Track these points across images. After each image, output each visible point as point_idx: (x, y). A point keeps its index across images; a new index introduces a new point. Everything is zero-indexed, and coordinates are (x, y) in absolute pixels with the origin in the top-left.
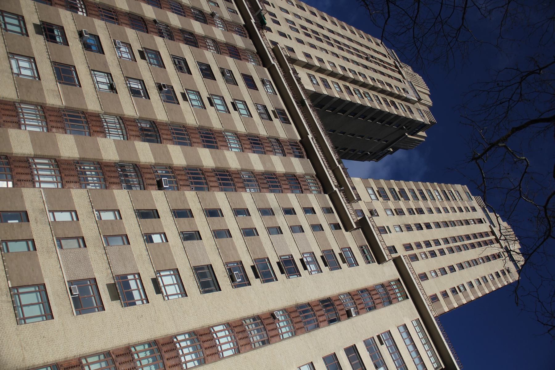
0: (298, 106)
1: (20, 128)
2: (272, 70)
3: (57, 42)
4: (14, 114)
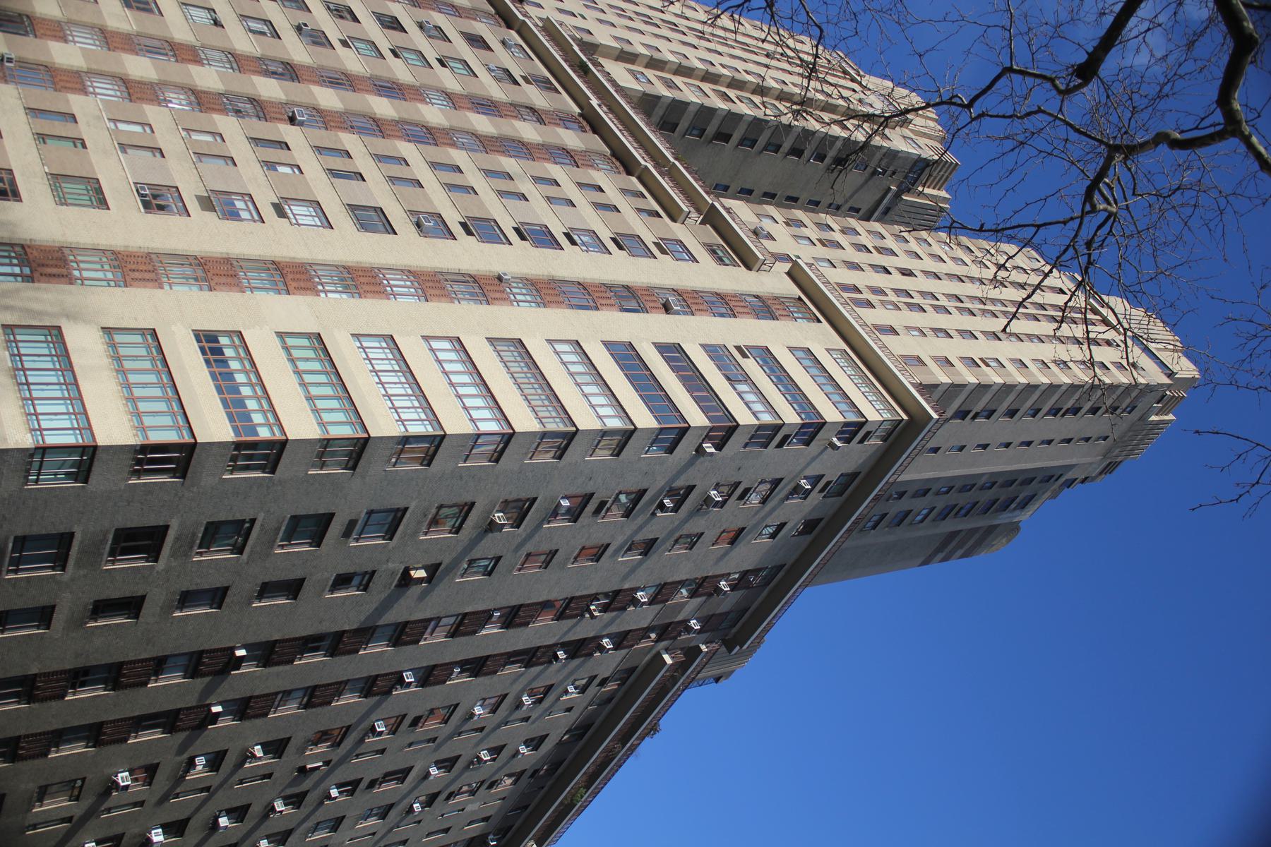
0: (579, 76)
1: (162, 288)
2: (644, 177)
3: (242, 220)
4: (150, 268)
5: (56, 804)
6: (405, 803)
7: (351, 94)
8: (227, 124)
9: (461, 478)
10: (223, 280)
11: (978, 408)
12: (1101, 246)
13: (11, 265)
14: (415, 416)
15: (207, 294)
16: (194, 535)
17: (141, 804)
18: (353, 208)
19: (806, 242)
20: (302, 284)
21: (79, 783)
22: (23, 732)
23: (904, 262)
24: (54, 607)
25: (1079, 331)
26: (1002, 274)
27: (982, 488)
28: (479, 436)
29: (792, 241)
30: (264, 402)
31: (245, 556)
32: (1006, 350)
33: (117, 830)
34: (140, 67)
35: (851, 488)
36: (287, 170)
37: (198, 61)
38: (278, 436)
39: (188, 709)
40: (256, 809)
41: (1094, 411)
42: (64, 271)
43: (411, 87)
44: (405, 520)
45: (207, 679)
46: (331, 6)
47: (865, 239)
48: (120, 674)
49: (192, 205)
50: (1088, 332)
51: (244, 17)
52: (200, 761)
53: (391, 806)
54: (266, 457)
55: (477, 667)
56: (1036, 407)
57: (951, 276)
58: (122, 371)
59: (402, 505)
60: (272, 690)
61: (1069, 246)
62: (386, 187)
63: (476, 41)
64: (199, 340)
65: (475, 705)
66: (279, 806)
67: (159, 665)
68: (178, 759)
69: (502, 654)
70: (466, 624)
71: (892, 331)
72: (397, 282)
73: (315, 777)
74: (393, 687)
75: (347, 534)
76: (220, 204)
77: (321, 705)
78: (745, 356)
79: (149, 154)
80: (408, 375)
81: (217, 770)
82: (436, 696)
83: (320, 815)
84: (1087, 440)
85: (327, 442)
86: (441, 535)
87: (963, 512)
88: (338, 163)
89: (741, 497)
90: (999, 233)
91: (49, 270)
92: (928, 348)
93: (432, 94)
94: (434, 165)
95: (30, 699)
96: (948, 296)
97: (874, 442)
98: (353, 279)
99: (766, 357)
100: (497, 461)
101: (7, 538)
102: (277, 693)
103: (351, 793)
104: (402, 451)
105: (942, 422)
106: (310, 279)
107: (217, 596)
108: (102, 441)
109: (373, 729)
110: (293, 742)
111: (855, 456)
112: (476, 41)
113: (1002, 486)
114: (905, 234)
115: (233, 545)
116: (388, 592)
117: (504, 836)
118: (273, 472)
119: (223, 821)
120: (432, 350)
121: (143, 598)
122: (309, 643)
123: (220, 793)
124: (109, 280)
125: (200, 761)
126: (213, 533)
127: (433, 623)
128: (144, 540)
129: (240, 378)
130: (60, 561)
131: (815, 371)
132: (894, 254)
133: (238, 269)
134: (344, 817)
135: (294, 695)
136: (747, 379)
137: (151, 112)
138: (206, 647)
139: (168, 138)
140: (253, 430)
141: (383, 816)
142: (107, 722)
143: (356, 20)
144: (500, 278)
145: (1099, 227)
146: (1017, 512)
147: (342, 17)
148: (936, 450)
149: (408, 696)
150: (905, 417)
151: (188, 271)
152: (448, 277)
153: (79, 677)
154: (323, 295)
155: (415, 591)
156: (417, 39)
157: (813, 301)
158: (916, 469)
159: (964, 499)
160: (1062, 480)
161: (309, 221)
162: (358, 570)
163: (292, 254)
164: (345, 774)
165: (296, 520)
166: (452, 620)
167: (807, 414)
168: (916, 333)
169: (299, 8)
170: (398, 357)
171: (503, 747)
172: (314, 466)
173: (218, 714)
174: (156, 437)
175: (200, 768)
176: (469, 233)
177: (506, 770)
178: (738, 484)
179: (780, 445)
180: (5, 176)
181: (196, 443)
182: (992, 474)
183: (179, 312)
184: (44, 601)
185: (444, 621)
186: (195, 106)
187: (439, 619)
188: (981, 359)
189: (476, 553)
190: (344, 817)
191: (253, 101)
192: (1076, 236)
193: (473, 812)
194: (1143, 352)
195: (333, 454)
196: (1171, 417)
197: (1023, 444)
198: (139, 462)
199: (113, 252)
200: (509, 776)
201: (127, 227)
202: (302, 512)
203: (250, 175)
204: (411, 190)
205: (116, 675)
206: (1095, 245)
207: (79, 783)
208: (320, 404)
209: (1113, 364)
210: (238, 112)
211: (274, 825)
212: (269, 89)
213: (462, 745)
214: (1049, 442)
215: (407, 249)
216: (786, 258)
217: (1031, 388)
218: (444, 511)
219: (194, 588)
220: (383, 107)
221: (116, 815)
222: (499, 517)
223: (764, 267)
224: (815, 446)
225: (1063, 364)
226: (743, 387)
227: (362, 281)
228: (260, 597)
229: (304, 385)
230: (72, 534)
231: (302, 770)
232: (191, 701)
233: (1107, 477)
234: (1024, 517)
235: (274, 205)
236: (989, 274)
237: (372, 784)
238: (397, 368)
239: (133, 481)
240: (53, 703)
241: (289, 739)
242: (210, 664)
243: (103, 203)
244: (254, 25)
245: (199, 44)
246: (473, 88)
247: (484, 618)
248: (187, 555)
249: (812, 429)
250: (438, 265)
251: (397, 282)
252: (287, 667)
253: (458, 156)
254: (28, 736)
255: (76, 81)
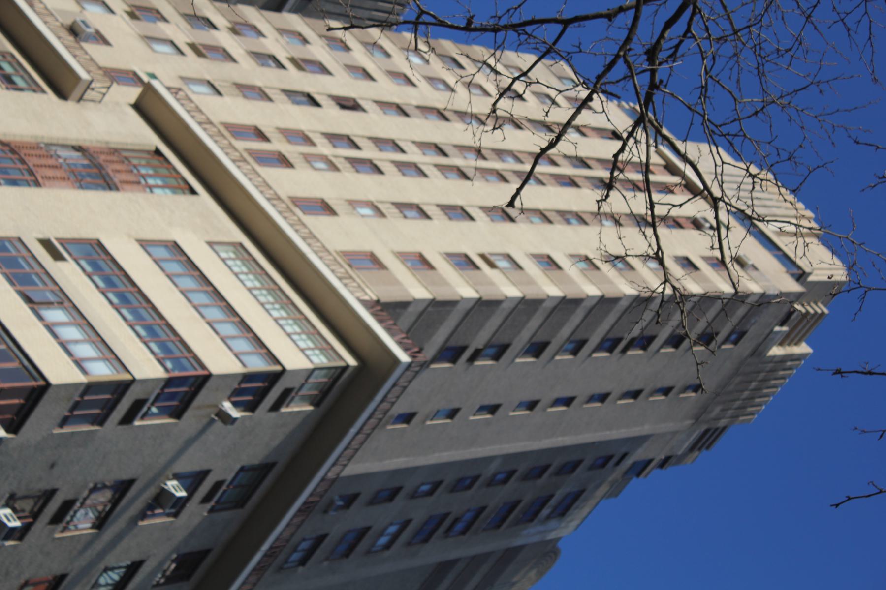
11: (479, 342)
12: (673, 56)
19: (167, 49)
23: (343, 84)
25: (638, 203)
26: (505, 104)
27: (492, 482)
29: (140, 47)
32: (523, 239)
35: (258, 492)
41: (676, 341)
47: (273, 44)
50: (652, 205)
56: (579, 336)
57: (426, 110)
61: (617, 56)
71: (326, 208)
78: (57, 256)
84: (666, 391)
87: (459, 526)
89: (58, 518)
90: (502, 31)
92: (388, 238)
96: (424, 146)
97: (299, 407)
99: (96, 257)
105: (417, 368)
111: (260, 435)
113: (526, 477)
114: (339, 34)
131: (188, 283)
132: (229, 57)
136: (64, 300)
145: (669, 24)
146: (553, 523)
148: (407, 418)
150: (352, 362)
157: (182, 156)
158: (374, 454)
159: (459, 504)
160: (628, 462)
167: (176, 361)
168: (367, 211)
178: (49, 494)
179: (128, 419)
182: (507, 458)
188: (483, 256)
192: (628, 40)
194: (750, 237)
196: (803, 348)
197: (557, 402)
206: (662, 56)
209: (694, 260)
214: (603, 398)
216: (133, 78)
217: (568, 304)
223: (89, 94)
224: (192, 418)
225: (618, 260)
226: (55, 315)
233: (703, 456)
234: (564, 531)
236: (482, 106)
249: (186, 388)
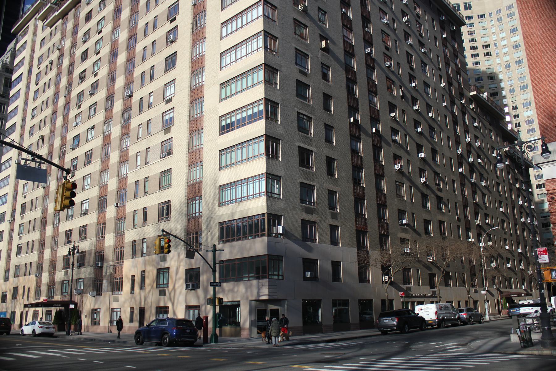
4: (194, 152)
5: (404, 192)
6: (421, 55)
7: (117, 72)
8: (134, 123)
9: (283, 24)
10: (198, 124)
13: (195, 204)
14: (256, 43)
15: (205, 130)
16: (303, 136)
17: (408, 161)
18: (166, 71)
20: (200, 91)
21: (398, 183)
22: (376, 202)
24: (329, 190)
28: (264, 15)
30: (249, 107)
31: (312, 116)
33: (417, 170)
34: (114, 157)
36: (152, 98)
37: (109, 135)
38: (263, 101)
39: (373, 142)
40: (416, 117)
42: (197, 184)
43: (112, 46)
44: (300, 49)
45: (362, 133)
46: (80, 81)
48: (357, 167)
49: (168, 136)
51: (89, 117)
52: (394, 138)
53: (422, 62)
54: (272, 107)
55: (366, 20)
58: (236, 163)
59: (294, 50)
60: (368, 108)
62: (156, 56)
63: (89, 16)
64: (223, 133)
65: (382, 22)
66: (416, 108)
67: (354, 152)
68: (392, 146)
69: (361, 8)
70: (347, 24)
72: (197, 51)
73: (406, 92)
74: (372, 58)
75: (305, 74)
76: (167, 125)
77: (376, 88)
79: (149, 153)
80: (237, 46)
81: (399, 131)
82: (377, 39)
83: (422, 92)
85: (266, 82)
86: (307, 34)
88: (147, 77)
91: (197, 190)
93: (106, 130)
94: (145, 35)
95: (363, 199)
98: (197, 70)
100: (276, 7)
101: (301, 206)
102: (370, 106)
103: (414, 78)
104: (270, 49)
106: (197, 88)
107: (328, 128)
108: (264, 171)
109: (389, 67)
110: (391, 101)
112: (89, 16)
115: (308, 121)
116: (331, 58)
117: (441, 13)
118: (278, 104)
119: (419, 130)
120: (227, 36)
121: (327, 157)
122: (350, 92)
123: (408, 130)
124: (200, 168)
125: (394, 138)
126: (303, 129)
127: (345, 39)
128: (304, 157)
129: (239, 117)
130: (311, 187)
133: (194, 118)
134: (424, 81)
135: (371, 99)
137: (132, 152)
138: (349, 133)
139: (141, 146)
140: (260, 112)
141: (426, 65)
142: (375, 172)
143: (85, 71)
144: (194, 5)
147: (85, 77)
149: (374, 51)
151: (195, 138)
152: (195, 29)
153: (356, 182)
154: (204, 83)
155: (331, 46)
156: (90, 44)
161: (172, 89)
162: (321, 70)
163: (187, 96)
164: (406, 80)
165: (298, 95)
166: (345, 31)
169: (83, 94)
170: (230, 51)
171: (402, 11)
172: (276, 87)
173: (376, 130)
174: (263, 150)
175: (397, 138)
176: (175, 19)
177: (413, 10)
180: (161, 206)
181: (268, 255)
183: (212, 141)
184: (326, 194)
185: (345, 34)
186: (128, 135)
187: (344, 36)
189: (316, 19)
190: (424, 81)
191: (124, 112)
193: (429, 26)
195: (271, 80)
198: (273, 157)
199: (189, 166)
200: (415, 9)
201: (178, 161)
202: (295, 93)
203: (155, 114)
204: (157, 46)
205: (357, 168)
207: (398, 183)
208: (250, 84)
210: (129, 118)
211: (423, 110)
212: (118, 106)
213: (399, 29)
215: (183, 46)
218: (297, 32)
219: (324, 137)
220: (122, 58)
221: (411, 170)
222: (301, 7)
227: (197, 66)
228: (329, 111)
229: (242, 91)
230: (301, 182)
231: (402, 97)
232: (370, 140)
235: (166, 103)
237: (412, 69)
238: (234, 51)
239: (280, 159)
240: (366, 191)
241: (389, 102)
242: (356, 133)
243: (170, 170)
244: (92, 113)
245: (102, 135)
246: (110, 18)
247: (345, 16)
248: (311, 139)
250: (189, 33)
251: (197, 51)
252: (359, 101)
253: (141, 24)
254: (377, 201)
255: (122, 181)
